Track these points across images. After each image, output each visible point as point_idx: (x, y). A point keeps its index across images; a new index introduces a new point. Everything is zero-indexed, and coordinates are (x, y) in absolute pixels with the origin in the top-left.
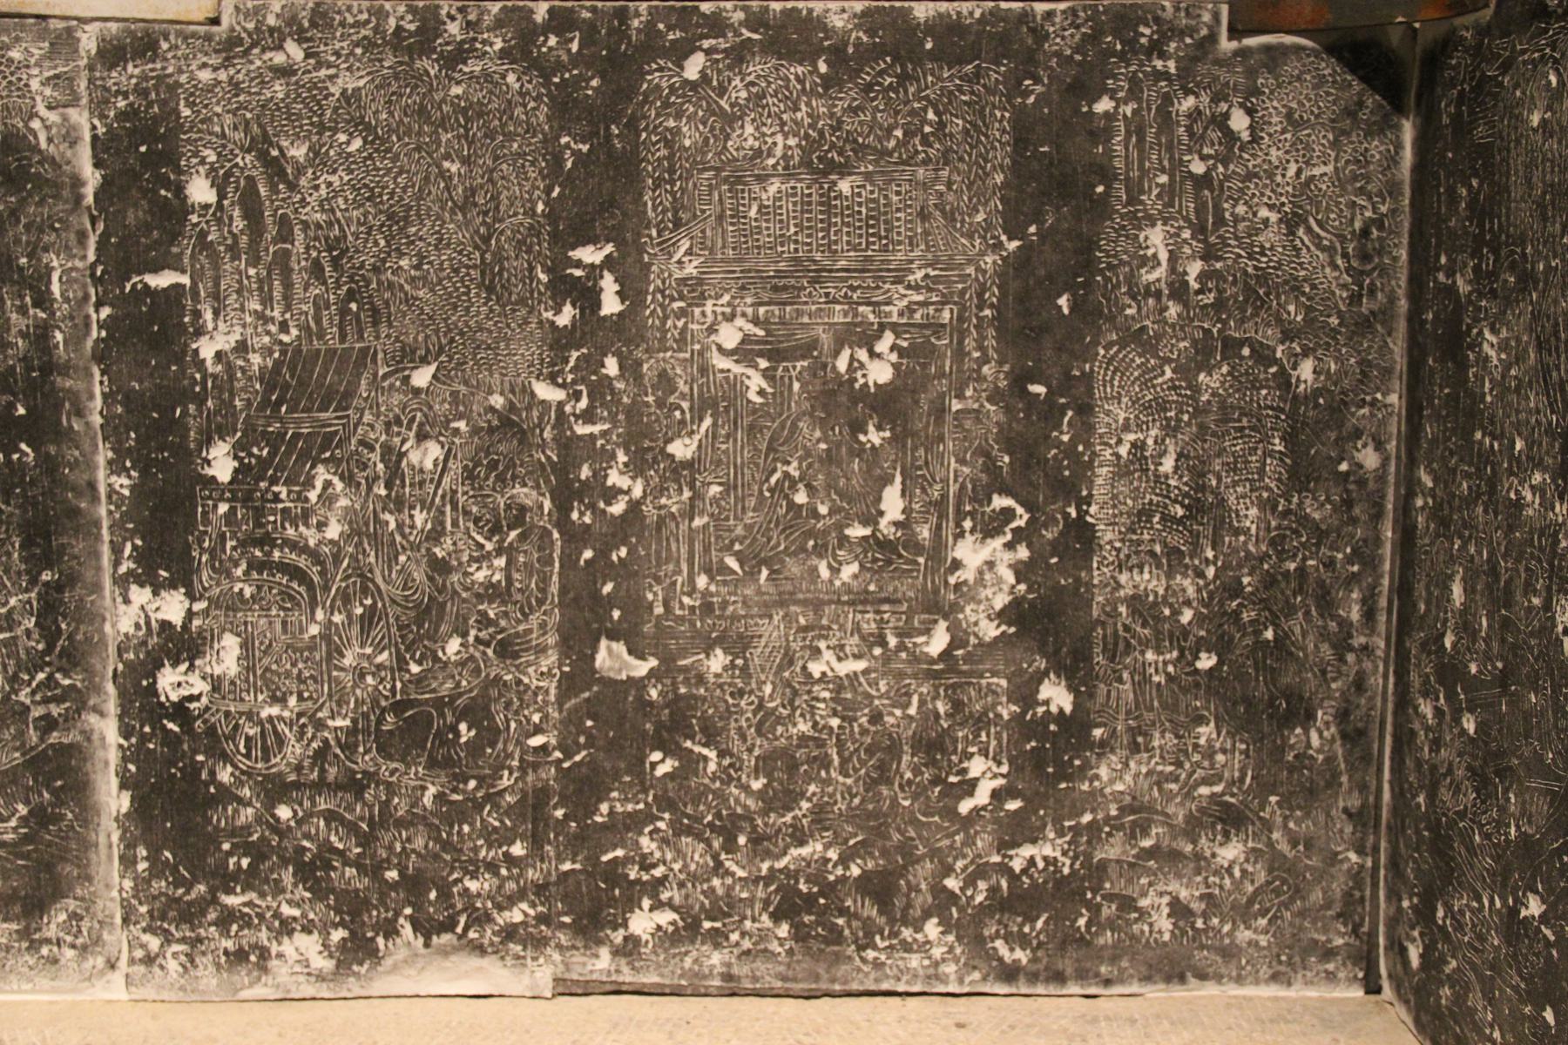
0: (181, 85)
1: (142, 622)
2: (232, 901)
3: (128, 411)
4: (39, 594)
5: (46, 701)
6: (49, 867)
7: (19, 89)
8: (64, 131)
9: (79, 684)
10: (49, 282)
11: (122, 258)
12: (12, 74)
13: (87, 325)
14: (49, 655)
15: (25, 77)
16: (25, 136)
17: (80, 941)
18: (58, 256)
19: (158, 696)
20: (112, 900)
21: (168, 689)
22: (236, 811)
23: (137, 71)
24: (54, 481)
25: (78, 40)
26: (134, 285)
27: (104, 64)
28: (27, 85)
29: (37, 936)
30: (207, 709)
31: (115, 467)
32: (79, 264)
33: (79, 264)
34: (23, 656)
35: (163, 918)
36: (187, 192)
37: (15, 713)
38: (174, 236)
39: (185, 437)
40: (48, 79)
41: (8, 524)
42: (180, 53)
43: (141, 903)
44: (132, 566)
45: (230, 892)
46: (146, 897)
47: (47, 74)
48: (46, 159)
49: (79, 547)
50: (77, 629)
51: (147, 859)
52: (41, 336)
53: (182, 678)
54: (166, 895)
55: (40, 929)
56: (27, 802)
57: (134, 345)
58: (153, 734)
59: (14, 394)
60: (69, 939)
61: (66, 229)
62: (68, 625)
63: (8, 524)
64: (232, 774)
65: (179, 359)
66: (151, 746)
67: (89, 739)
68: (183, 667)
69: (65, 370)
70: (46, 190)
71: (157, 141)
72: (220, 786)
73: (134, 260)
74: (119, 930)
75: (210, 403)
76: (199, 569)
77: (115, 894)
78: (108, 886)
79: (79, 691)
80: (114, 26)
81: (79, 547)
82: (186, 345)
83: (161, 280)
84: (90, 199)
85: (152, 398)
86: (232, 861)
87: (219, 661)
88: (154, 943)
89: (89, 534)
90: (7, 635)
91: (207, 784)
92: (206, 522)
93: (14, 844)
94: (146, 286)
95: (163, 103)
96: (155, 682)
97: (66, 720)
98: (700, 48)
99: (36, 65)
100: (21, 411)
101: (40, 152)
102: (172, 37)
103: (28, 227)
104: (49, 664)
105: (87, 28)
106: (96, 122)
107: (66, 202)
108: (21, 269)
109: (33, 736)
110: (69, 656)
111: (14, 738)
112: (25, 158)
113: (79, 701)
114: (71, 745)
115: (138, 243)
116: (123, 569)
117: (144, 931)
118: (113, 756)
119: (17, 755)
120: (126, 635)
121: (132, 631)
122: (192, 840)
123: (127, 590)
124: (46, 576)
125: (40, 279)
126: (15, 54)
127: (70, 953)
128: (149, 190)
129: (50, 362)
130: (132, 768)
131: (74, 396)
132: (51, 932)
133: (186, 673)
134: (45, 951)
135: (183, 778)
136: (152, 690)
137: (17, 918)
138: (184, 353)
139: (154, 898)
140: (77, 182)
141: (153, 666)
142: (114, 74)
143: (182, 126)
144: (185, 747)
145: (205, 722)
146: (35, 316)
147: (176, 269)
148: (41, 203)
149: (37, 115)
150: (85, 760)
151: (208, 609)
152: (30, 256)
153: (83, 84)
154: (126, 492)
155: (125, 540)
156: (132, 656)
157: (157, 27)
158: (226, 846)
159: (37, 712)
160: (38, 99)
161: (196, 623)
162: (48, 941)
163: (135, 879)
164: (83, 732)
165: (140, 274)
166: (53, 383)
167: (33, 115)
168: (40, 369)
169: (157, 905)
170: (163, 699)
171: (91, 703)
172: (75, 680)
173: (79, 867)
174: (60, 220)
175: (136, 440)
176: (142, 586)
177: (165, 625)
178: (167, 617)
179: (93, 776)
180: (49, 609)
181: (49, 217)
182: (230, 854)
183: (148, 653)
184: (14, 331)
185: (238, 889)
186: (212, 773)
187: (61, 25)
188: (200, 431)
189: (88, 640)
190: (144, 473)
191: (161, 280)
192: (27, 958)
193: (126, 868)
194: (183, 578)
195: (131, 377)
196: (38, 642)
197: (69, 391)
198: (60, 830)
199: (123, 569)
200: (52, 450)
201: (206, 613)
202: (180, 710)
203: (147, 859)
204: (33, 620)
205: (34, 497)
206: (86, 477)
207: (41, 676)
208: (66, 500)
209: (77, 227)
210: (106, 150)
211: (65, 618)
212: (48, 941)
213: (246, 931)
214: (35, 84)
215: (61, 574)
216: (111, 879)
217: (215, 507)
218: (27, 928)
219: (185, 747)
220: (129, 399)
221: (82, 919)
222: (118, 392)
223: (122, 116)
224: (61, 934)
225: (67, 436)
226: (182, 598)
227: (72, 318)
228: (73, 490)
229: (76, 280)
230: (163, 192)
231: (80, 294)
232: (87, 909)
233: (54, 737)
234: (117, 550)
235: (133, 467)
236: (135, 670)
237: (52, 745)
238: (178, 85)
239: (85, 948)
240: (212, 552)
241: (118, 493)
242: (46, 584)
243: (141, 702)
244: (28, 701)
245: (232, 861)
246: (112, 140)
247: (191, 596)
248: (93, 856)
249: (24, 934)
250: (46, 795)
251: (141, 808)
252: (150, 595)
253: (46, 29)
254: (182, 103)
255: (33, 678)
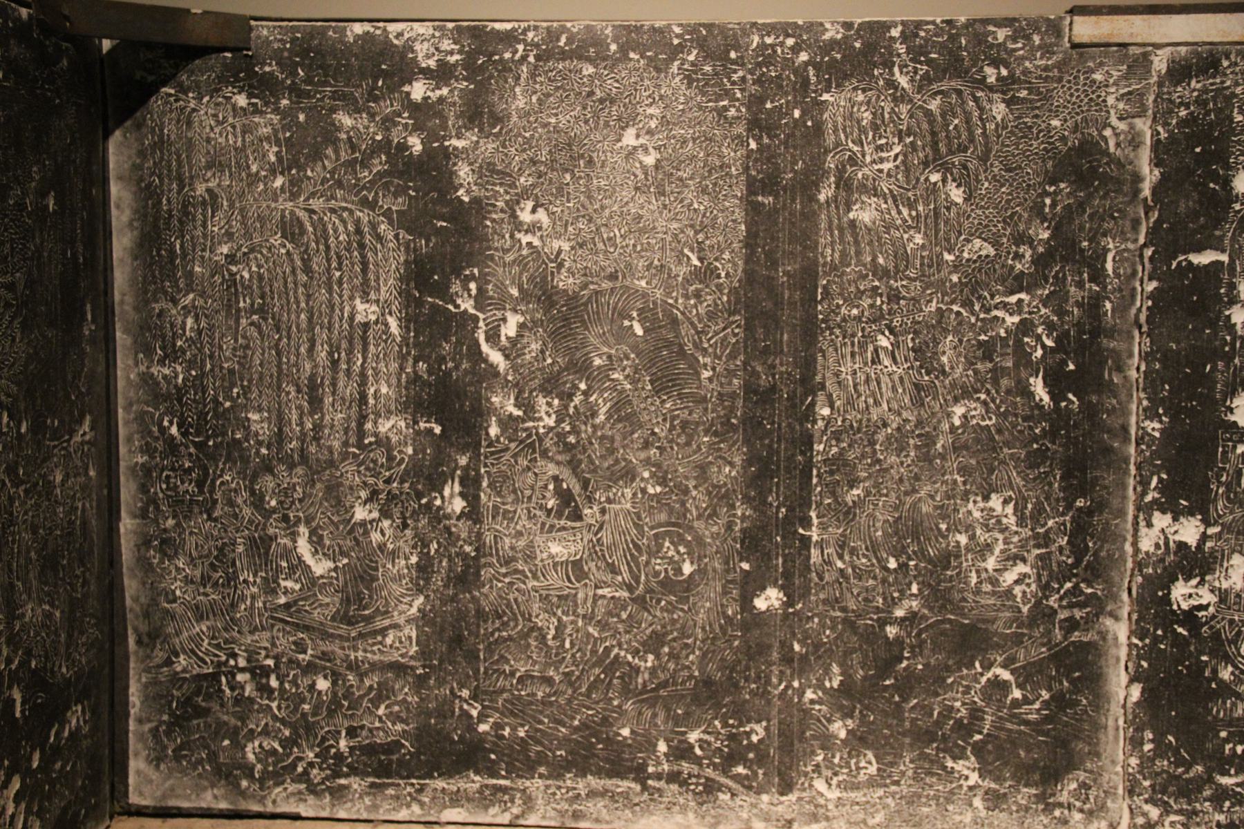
0: (1236, 96)
1: (1161, 543)
2: (1226, 781)
3: (1164, 367)
4: (1073, 517)
5: (1071, 606)
6: (1064, 744)
7: (1097, 104)
8: (1130, 137)
9: (1099, 593)
10: (1105, 261)
11: (1171, 239)
12: (1093, 92)
13: (1133, 296)
14: (1076, 568)
15: (1103, 94)
16: (1098, 142)
17: (1087, 806)
18: (1114, 239)
19: (1171, 605)
20: (1117, 773)
21: (1180, 599)
22: (1234, 705)
23: (1199, 86)
24: (1093, 425)
25: (1152, 62)
26: (1180, 263)
27: (1171, 81)
28: (1104, 101)
29: (1051, 800)
30: (1214, 617)
31: (1150, 414)
32: (1131, 246)
33: (1131, 246)
34: (1055, 569)
35: (1163, 792)
36: (1233, 185)
37: (1044, 615)
38: (1217, 222)
39: (1212, 388)
40: (1123, 95)
41: (1053, 459)
42: (1237, 69)
43: (1145, 779)
44: (1157, 496)
45: (1225, 773)
46: (1150, 773)
47: (1122, 91)
48: (1112, 160)
49: (1110, 479)
50: (1102, 546)
51: (1152, 741)
52: (1093, 306)
53: (1192, 591)
54: (1167, 772)
55: (1054, 795)
56: (1049, 689)
57: (1175, 312)
58: (1164, 636)
59: (1067, 353)
60: (1078, 804)
61: (1123, 217)
62: (1095, 543)
63: (1053, 459)
64: (1232, 673)
65: (1213, 324)
66: (1162, 647)
67: (1104, 639)
68: (1194, 582)
69: (1111, 333)
70: (1110, 186)
71: (1211, 143)
72: (1221, 682)
73: (1182, 242)
74: (1121, 800)
75: (1237, 361)
76: (1215, 500)
77: (1119, 769)
78: (1113, 762)
79: (1098, 598)
80: (1183, 50)
81: (1110, 479)
82: (1220, 312)
83: (1204, 258)
84: (1146, 192)
85: (1187, 356)
86: (1228, 747)
87: (1227, 577)
88: (1154, 813)
89: (1120, 468)
90: (1044, 551)
91: (1209, 681)
92: (1225, 459)
93: (1037, 723)
94: (1190, 263)
95: (1219, 111)
96: (1169, 593)
97: (1086, 623)
98: (998, 68)
99: (1114, 84)
100: (1072, 367)
101: (1109, 155)
102: (1233, 57)
103: (1091, 216)
104: (1076, 575)
105: (1159, 52)
106: (1160, 129)
107: (1125, 195)
108: (1082, 251)
109: (1058, 634)
110: (1093, 569)
111: (1042, 635)
112: (1096, 160)
113: (1098, 607)
114: (1089, 643)
115: (1186, 228)
116: (1148, 498)
117: (1146, 801)
118: (1123, 653)
119: (1044, 649)
120: (1147, 553)
121: (1152, 550)
122: (1193, 727)
123: (1151, 516)
124: (1080, 503)
125: (1098, 257)
126: (1098, 77)
127: (1078, 816)
128: (1200, 184)
129: (1099, 326)
130: (1145, 664)
131: (1116, 354)
132: (1064, 797)
133: (1196, 587)
134: (1057, 813)
135: (1188, 675)
136: (1166, 600)
137: (1036, 785)
138: (1218, 319)
139: (1157, 774)
140: (1137, 178)
141: (1169, 579)
142: (1179, 89)
143: (1234, 129)
144: (1192, 648)
145: (1211, 628)
146: (1091, 289)
147: (1216, 249)
148: (1104, 197)
149: (1110, 125)
150: (1100, 656)
151: (1220, 533)
152: (1090, 241)
153: (1151, 98)
154: (1157, 434)
155: (1152, 474)
156: (1151, 571)
157: (1220, 48)
158: (1223, 734)
159: (1063, 615)
160: (1112, 112)
161: (1209, 544)
162: (1060, 805)
163: (1140, 758)
164: (1099, 633)
165: (1185, 253)
166: (1099, 344)
167: (1107, 125)
168: (1090, 333)
169: (1159, 780)
170: (1175, 607)
171: (1109, 608)
172: (1098, 589)
173: (1090, 744)
174: (1119, 211)
175: (1170, 391)
176: (1164, 512)
177: (1182, 546)
178: (1183, 539)
179: (1105, 670)
180: (1080, 531)
181: (1110, 208)
182: (1227, 740)
183: (1165, 569)
184: (1071, 301)
185: (1232, 772)
186: (1215, 672)
187: (1138, 51)
188: (1226, 385)
189: (1110, 556)
190: (1174, 418)
191: (1204, 258)
192: (1042, 817)
193: (1134, 748)
194: (1201, 508)
195: (1171, 339)
196: (1068, 557)
197: (1113, 350)
198: (1076, 713)
199: (1148, 498)
200: (1094, 399)
201: (1219, 536)
202: (1189, 618)
203: (1152, 741)
204: (1066, 538)
205: (1076, 438)
206: (1120, 422)
207: (1068, 585)
208: (1103, 440)
209: (1132, 215)
210: (1167, 152)
211: (1092, 538)
212: (1060, 805)
213: (1237, 808)
214: (1111, 100)
215: (1092, 501)
216: (1117, 756)
217: (1235, 447)
218: (1044, 793)
219: (1192, 648)
220: (1167, 358)
221: (1090, 788)
222: (1157, 352)
223: (1183, 123)
224: (1072, 800)
225: (1111, 389)
226: (1198, 523)
227: (1120, 290)
228: (1108, 432)
229: (1127, 259)
230: (1212, 185)
231: (1129, 271)
232: (1095, 780)
233: (1076, 636)
234: (1144, 483)
235: (1165, 414)
236: (1153, 583)
237: (1073, 642)
238: (1234, 95)
239: (1091, 813)
240: (1228, 486)
241: (1149, 435)
242: (1080, 509)
243: (1154, 606)
244: (1056, 606)
245: (1228, 747)
246: (1172, 143)
247: (1207, 522)
248: (1102, 736)
249: (1041, 798)
250: (1066, 684)
251: (1150, 700)
252: (1170, 521)
253: (1126, 55)
254: (1236, 110)
255: (1062, 587)
